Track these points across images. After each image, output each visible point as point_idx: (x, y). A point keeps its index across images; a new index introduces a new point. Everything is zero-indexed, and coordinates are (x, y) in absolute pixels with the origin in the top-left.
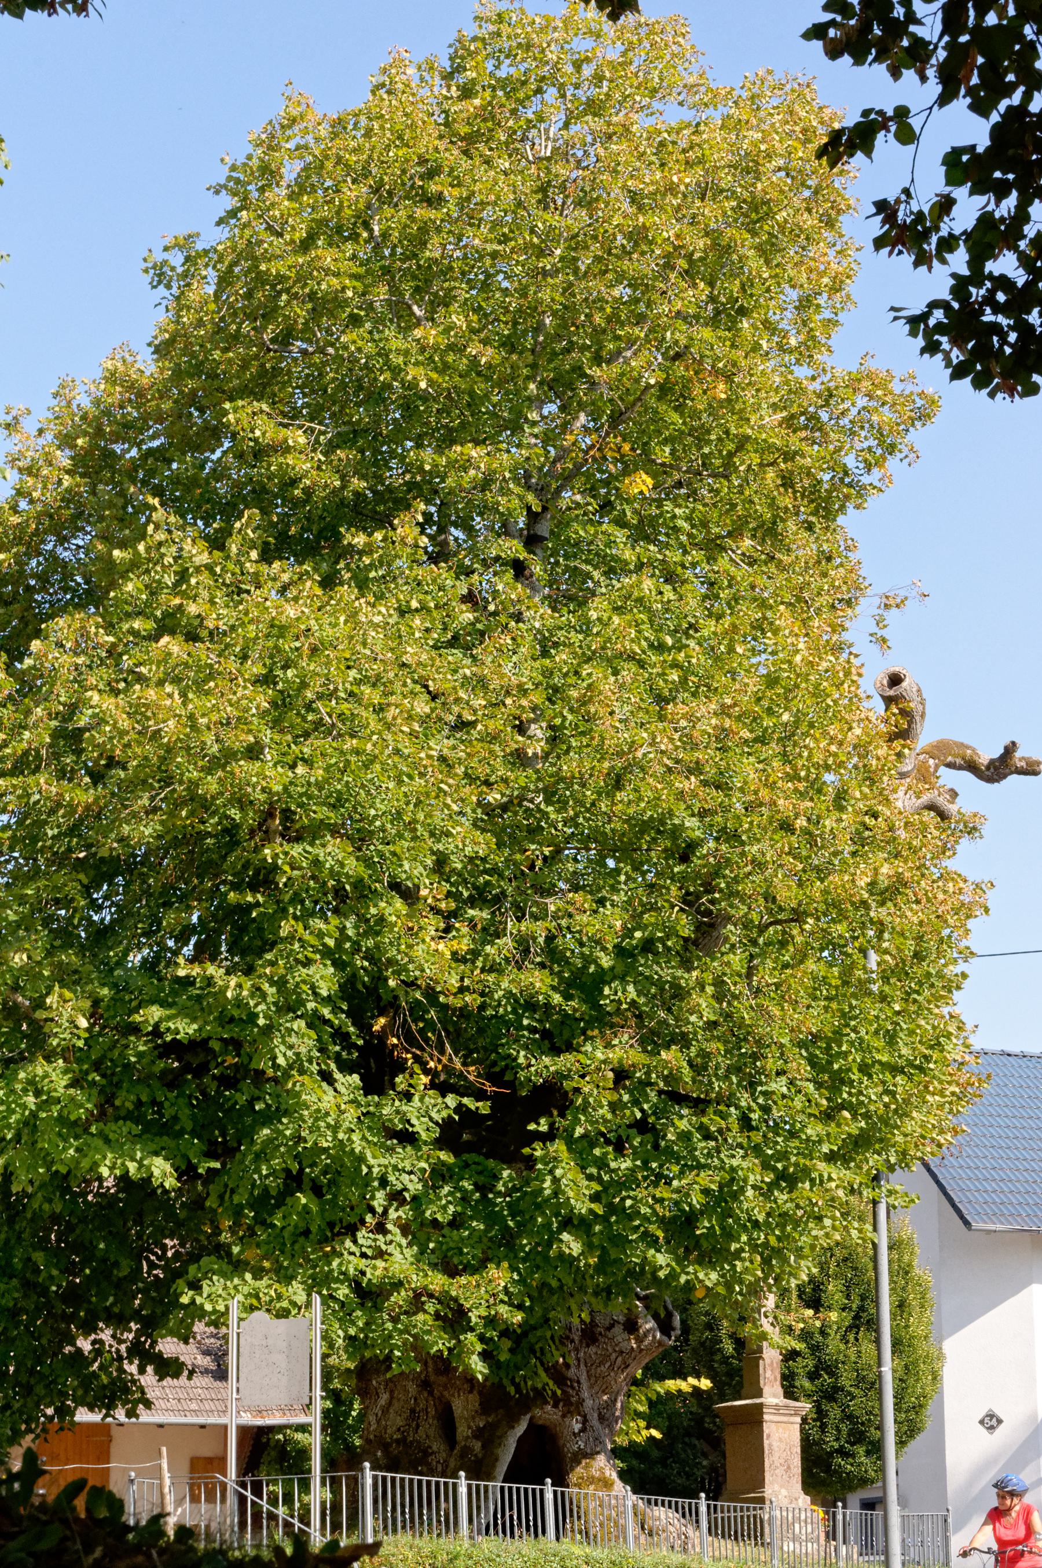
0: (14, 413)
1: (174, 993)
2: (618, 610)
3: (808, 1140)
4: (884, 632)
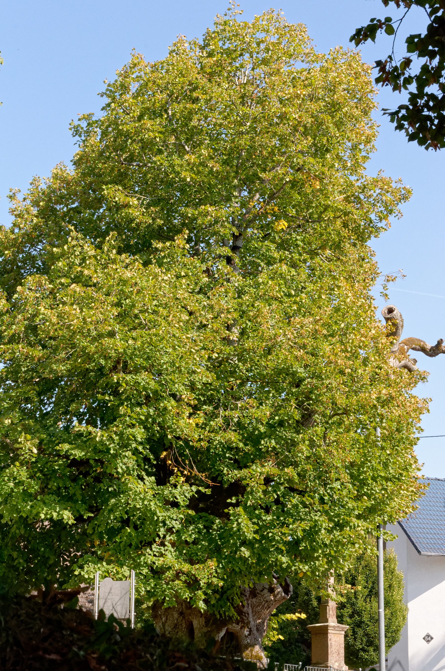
0: (13, 191)
1: (75, 439)
2: (272, 279)
3: (349, 508)
4: (387, 292)
